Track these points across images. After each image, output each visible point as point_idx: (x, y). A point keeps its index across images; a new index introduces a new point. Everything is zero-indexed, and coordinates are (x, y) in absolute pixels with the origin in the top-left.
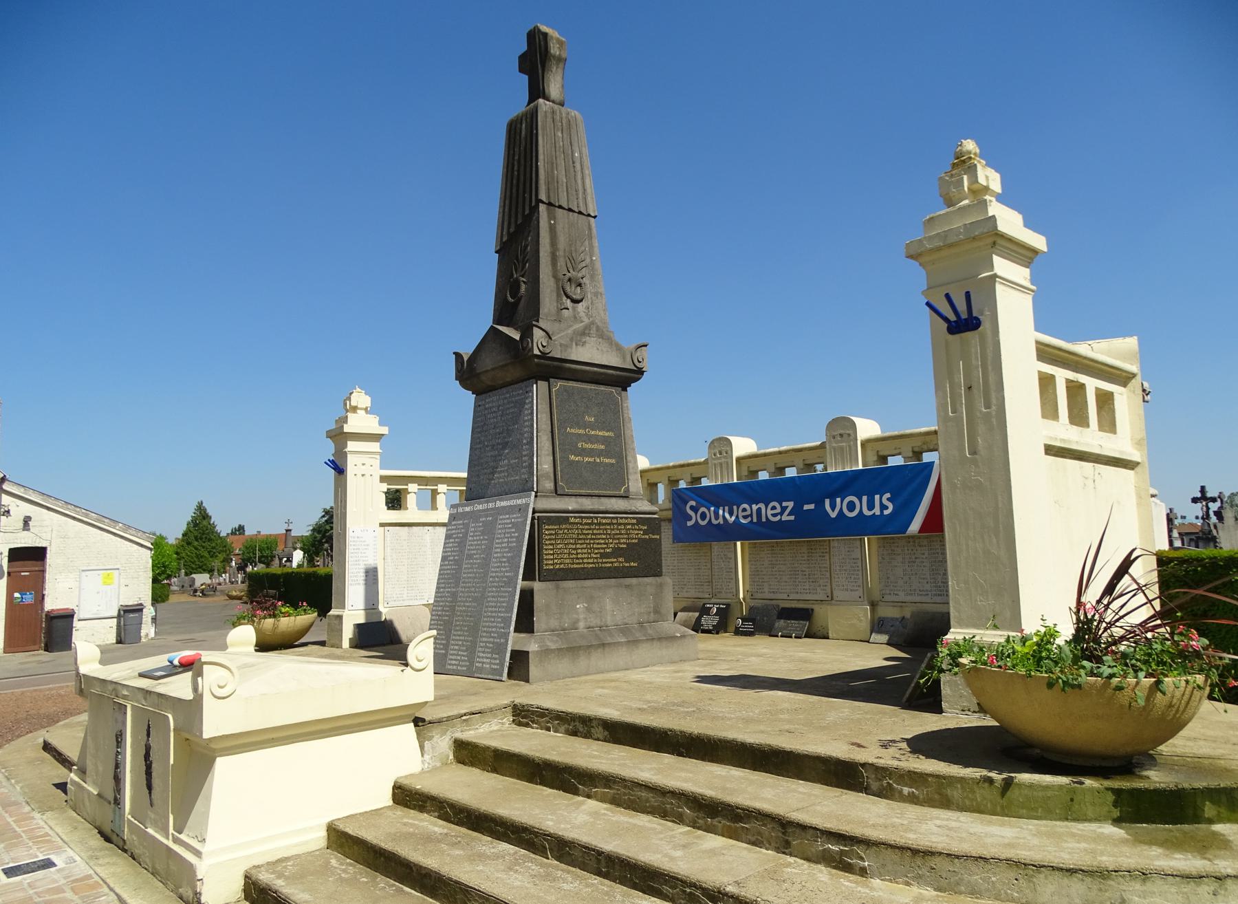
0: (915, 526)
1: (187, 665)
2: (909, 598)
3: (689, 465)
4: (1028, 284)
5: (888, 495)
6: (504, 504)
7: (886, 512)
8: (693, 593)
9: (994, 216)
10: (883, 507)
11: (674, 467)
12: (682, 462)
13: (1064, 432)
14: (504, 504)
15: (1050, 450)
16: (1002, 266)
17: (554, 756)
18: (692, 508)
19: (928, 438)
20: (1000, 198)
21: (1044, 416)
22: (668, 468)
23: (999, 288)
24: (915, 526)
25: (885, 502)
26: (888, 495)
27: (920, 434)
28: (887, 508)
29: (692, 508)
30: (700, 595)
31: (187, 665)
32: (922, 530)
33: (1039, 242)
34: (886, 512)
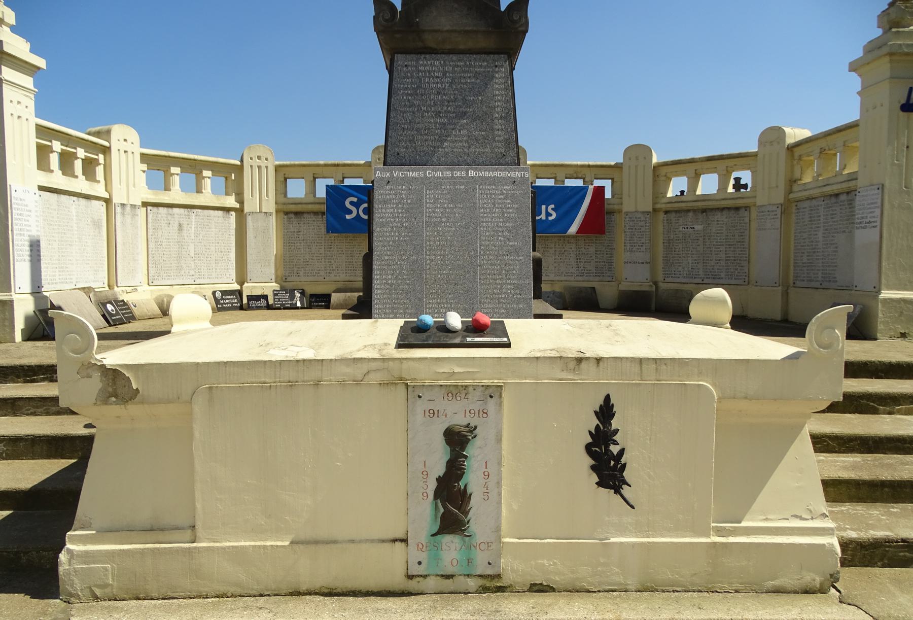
0: (573, 229)
1: (410, 577)
2: (557, 278)
3: (345, 165)
4: (32, 87)
5: (553, 206)
6: (486, 174)
7: (550, 218)
8: (342, 277)
9: (879, 27)
10: (548, 214)
11: (326, 165)
12: (336, 162)
13: (57, 179)
14: (486, 174)
15: (41, 188)
16: (8, 73)
17: (886, 475)
18: (352, 203)
19: (579, 169)
20: (13, 29)
21: (38, 169)
22: (318, 165)
23: (6, 88)
24: (573, 229)
25: (550, 210)
26: (553, 206)
27: (577, 166)
28: (551, 215)
29: (352, 203)
30: (352, 278)
31: (410, 577)
32: (581, 230)
33: (41, 62)
34: (550, 218)
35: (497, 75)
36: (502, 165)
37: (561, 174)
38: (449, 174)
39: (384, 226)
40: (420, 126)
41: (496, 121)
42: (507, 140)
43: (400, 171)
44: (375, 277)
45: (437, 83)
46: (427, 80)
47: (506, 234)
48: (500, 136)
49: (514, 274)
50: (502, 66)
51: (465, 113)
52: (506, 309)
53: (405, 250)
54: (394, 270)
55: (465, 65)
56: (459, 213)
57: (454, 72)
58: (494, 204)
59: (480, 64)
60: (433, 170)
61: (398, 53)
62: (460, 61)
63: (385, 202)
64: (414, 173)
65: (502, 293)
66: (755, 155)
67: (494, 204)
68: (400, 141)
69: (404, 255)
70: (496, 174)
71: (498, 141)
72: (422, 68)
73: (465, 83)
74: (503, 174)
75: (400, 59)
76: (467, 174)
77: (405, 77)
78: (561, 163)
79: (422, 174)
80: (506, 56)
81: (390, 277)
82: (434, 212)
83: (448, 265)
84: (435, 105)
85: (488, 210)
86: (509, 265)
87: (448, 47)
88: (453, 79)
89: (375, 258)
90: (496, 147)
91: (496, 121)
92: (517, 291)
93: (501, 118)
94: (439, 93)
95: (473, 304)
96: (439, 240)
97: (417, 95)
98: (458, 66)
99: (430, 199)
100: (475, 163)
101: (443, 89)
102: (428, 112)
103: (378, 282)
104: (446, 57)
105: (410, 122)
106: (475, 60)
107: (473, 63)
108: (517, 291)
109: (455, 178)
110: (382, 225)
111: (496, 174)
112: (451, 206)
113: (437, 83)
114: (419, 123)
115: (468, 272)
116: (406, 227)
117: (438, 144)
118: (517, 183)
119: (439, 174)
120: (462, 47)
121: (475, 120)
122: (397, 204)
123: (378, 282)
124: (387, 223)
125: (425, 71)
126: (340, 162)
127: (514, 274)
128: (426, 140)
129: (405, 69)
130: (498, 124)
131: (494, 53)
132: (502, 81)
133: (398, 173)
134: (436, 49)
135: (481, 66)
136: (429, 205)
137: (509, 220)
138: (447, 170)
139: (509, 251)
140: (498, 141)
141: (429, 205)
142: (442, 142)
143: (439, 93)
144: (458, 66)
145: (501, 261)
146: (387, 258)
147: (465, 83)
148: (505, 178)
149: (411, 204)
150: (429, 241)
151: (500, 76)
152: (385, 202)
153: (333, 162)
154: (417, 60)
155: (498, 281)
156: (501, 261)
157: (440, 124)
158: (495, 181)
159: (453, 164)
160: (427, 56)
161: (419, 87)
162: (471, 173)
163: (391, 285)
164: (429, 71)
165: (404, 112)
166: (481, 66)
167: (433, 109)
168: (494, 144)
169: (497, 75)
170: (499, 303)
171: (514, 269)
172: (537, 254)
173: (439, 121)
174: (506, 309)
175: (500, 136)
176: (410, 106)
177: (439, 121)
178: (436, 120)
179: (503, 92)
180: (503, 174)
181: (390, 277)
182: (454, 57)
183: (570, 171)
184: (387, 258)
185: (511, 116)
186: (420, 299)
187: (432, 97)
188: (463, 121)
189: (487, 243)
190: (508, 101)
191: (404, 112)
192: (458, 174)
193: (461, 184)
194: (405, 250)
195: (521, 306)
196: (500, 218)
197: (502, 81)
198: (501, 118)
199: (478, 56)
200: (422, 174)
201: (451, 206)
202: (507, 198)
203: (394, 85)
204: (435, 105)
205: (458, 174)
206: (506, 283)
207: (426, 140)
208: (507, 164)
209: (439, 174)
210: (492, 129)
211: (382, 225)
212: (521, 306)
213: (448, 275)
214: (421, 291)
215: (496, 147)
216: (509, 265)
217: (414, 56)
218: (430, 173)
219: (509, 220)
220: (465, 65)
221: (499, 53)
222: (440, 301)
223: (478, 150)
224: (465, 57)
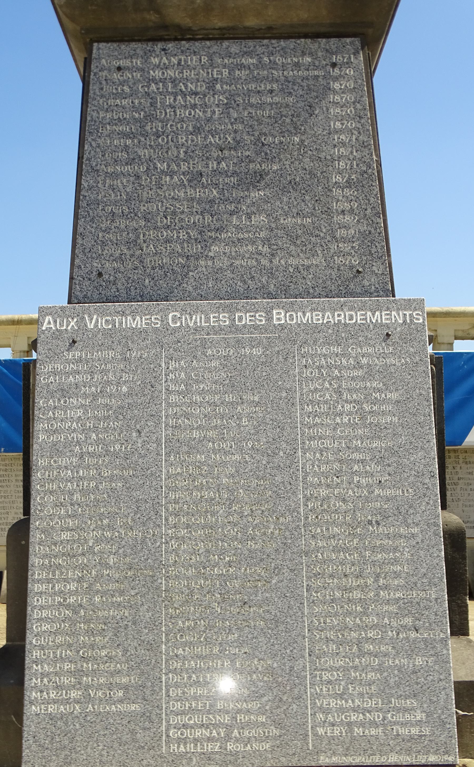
6: (317, 318)
14: (317, 318)
35: (336, 86)
36: (353, 294)
37: (445, 333)
38: (224, 319)
39: (60, 453)
40: (153, 207)
41: (337, 192)
42: (364, 235)
43: (102, 314)
44: (34, 587)
45: (194, 106)
46: (169, 100)
47: (372, 467)
48: (346, 227)
49: (397, 575)
50: (349, 63)
51: (261, 175)
52: (380, 669)
53: (112, 516)
54: (83, 567)
55: (260, 65)
56: (250, 418)
57: (232, 80)
58: (339, 392)
59: (296, 60)
60: (183, 311)
61: (99, 41)
62: (248, 54)
63: (64, 392)
64: (136, 319)
65: (366, 628)
66: (456, 338)
67: (339, 392)
68: (104, 243)
69: (111, 527)
70: (342, 317)
71: (344, 240)
72: (158, 74)
73: (261, 106)
74: (358, 317)
75: (106, 55)
76: (269, 319)
77: (116, 96)
78: (445, 308)
79: (155, 321)
80: (357, 42)
81: (72, 586)
82: (187, 416)
83: (222, 553)
84: (189, 156)
85: (324, 408)
86: (383, 549)
87: (218, 23)
88: (231, 96)
89: (36, 536)
90: (339, 253)
91: (337, 192)
92: (408, 621)
93: (349, 184)
94: (197, 130)
95: (293, 658)
96: (200, 488)
97: (146, 135)
98: (242, 67)
99: (176, 382)
100: (287, 290)
101: (209, 120)
102: (172, 174)
103: (42, 601)
104: (215, 47)
105: (128, 200)
106: (284, 52)
107: (279, 59)
108: (408, 621)
109: (238, 330)
110: (55, 450)
111: (342, 317)
112: (229, 398)
113: (194, 106)
114: (149, 201)
115: (277, 570)
116: (116, 455)
117: (197, 248)
118: (395, 338)
119: (198, 319)
120: (252, 22)
121: (284, 190)
122: (95, 397)
123: (42, 601)
124: (68, 444)
125: (163, 81)
126: (24, 317)
127: (397, 575)
128: (167, 241)
129: (116, 76)
130: (341, 199)
131: (327, 36)
132: (350, 97)
133: (97, 320)
134: (189, 30)
135: (297, 65)
136: (173, 398)
137: (377, 431)
138: (217, 310)
139: (380, 512)
140: (344, 240)
141: (173, 398)
142: (206, 244)
143: (197, 130)
144: (242, 67)
145: (362, 538)
146: (65, 536)
147: (261, 106)
148: (364, 327)
149: (129, 394)
150: (175, 489)
151: (343, 86)
152: (64, 392)
153: (10, 316)
154: (146, 56)
155: (357, 594)
156: (362, 538)
157: (200, 201)
158: (342, 335)
159: (233, 295)
160: (170, 45)
161: (150, 117)
162: (280, 316)
163: (75, 609)
164: (173, 81)
165: (114, 176)
166: (297, 65)
167: (184, 167)
168: (333, 247)
169: (336, 86)
170: (362, 654)
171: (396, 561)
172: (454, 519)
173: (198, 193)
174: (380, 669)
175: (346, 227)
176: (130, 162)
177: (198, 193)
178: (190, 192)
179: (351, 125)
180: (358, 317)
181: (72, 586)
182: (235, 47)
183: (464, 325)
184: (65, 536)
185: (370, 180)
186: (152, 647)
187: (182, 139)
188: (255, 195)
189: (323, 492)
190: (364, 145)
191: (114, 176)
192: (247, 319)
193: (253, 344)
194: (112, 516)
195: (419, 661)
196: (354, 426)
197: (350, 97)
198: (349, 184)
199: (291, 43)
200: (155, 321)
201: (229, 398)
202: (370, 373)
203: (92, 113)
204: (189, 156)
205: (247, 319)
206: (376, 599)
207: (167, 241)
208: (367, 293)
209: (198, 319)
210: (328, 212)
211: (55, 450)
212: (419, 661)
213: (224, 578)
214: (154, 624)
215: (339, 253)
216: (383, 549)
217: (139, 47)
218: (175, 317)
219: (377, 431)
220: (260, 65)
221: (340, 36)
222: (205, 651)
223: (293, 261)
224: (259, 46)
